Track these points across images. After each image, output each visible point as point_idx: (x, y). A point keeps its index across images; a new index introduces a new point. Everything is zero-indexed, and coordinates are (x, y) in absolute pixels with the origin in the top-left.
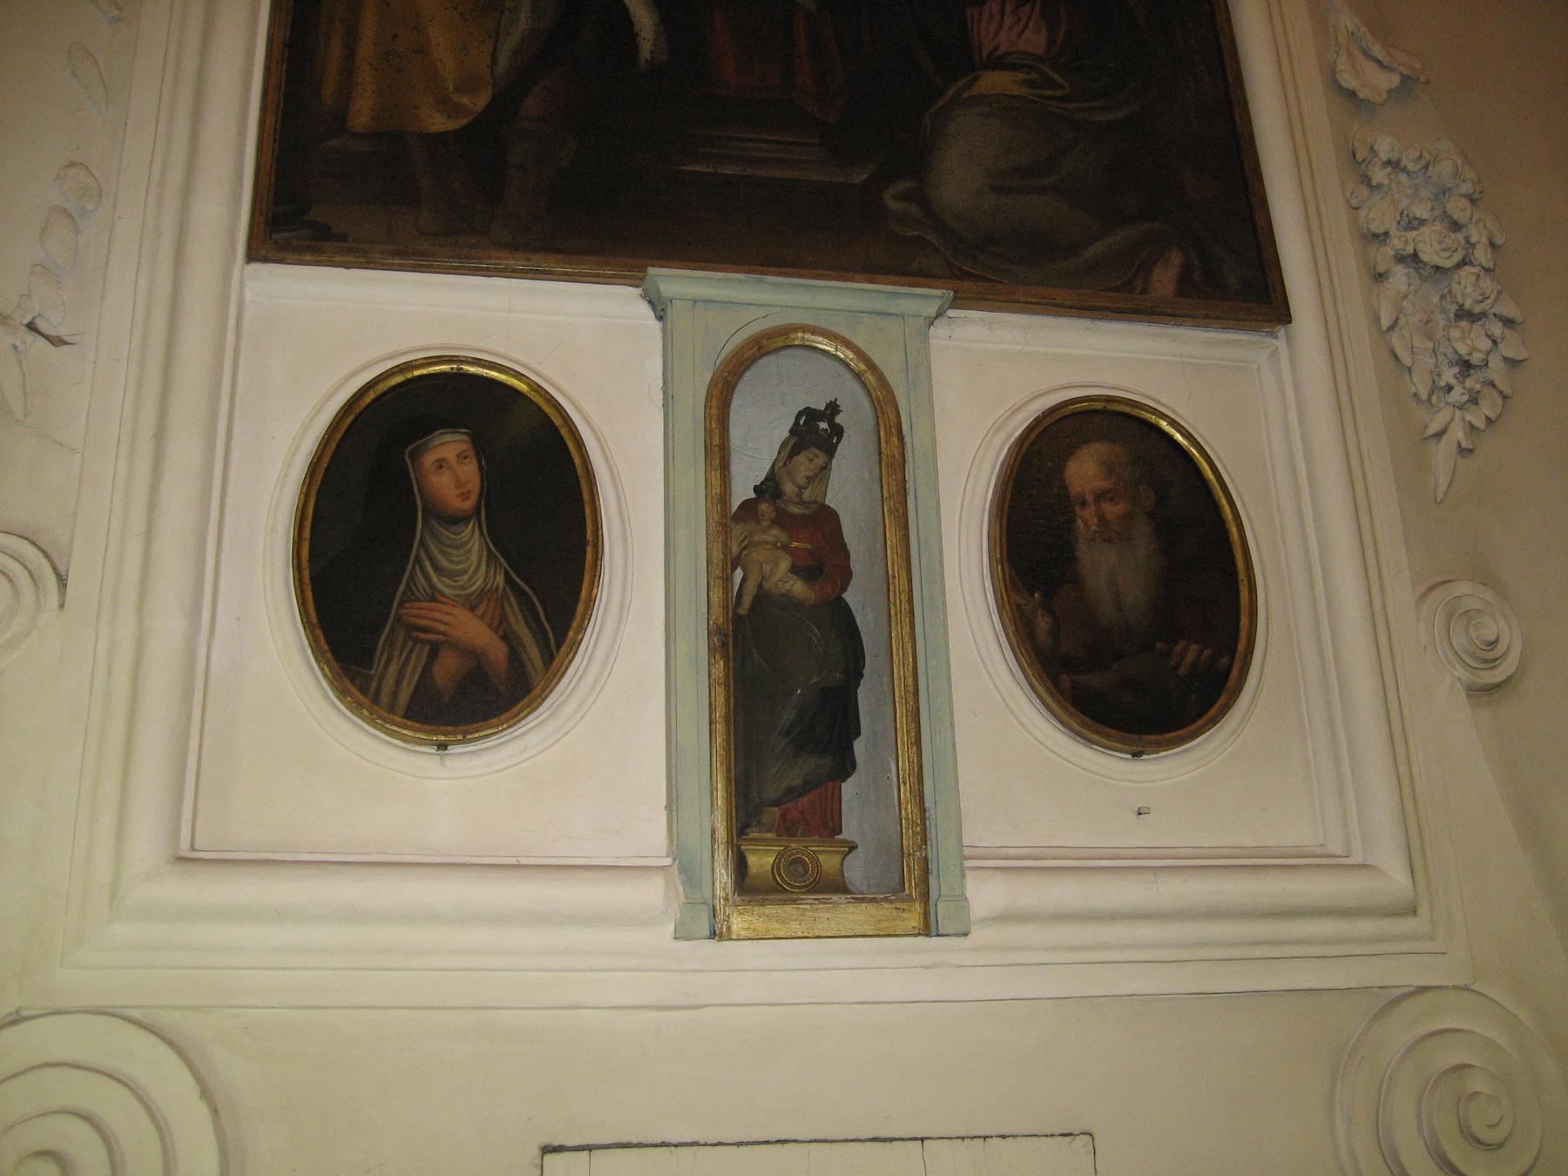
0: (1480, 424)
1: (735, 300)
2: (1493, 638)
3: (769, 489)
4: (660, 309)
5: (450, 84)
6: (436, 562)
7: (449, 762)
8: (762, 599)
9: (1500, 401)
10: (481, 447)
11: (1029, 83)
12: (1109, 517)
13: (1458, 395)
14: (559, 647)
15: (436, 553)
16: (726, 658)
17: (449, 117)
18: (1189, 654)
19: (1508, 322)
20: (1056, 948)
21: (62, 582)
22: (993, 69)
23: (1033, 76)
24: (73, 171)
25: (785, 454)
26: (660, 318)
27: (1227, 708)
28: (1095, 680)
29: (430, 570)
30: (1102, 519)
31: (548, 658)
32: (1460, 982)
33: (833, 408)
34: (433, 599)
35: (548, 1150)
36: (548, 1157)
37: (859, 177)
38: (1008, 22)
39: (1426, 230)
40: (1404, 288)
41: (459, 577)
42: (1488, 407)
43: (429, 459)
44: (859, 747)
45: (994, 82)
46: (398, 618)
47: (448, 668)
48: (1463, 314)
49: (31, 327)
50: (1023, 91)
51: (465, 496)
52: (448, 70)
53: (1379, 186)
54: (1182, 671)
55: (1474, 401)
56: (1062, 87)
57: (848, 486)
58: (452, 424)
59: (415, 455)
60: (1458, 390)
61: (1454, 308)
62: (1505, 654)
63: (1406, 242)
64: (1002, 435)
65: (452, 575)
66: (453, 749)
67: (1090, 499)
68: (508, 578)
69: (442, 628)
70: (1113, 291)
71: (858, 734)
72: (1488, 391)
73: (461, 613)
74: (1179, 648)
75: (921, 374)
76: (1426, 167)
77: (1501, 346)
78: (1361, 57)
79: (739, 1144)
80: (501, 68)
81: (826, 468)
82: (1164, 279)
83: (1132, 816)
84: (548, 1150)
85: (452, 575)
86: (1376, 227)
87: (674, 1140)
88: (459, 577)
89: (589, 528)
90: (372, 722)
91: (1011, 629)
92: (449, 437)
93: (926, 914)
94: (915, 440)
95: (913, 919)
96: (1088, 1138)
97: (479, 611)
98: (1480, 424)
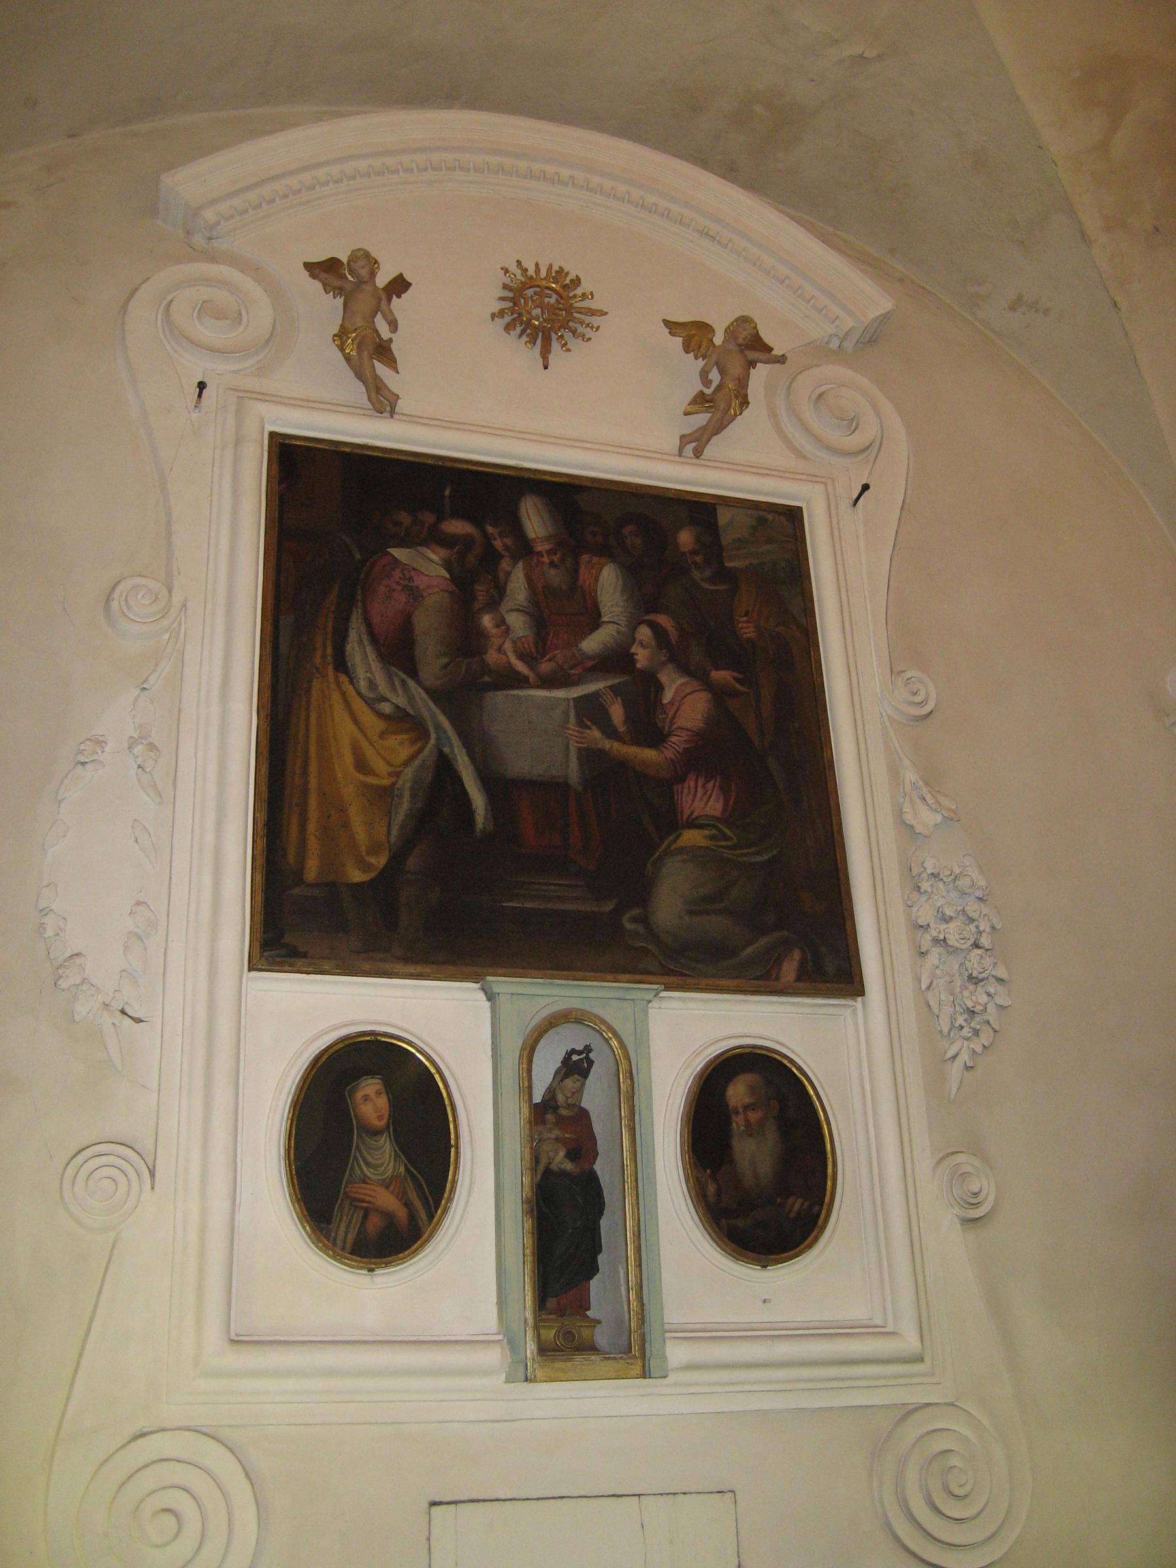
0: (979, 1049)
1: (536, 996)
2: (976, 1191)
3: (551, 1093)
4: (491, 997)
5: (363, 848)
6: (364, 1157)
7: (378, 1280)
8: (548, 1172)
9: (992, 1034)
10: (388, 1086)
11: (712, 838)
12: (752, 1121)
13: (966, 1032)
14: (437, 1209)
15: (366, 1154)
16: (532, 1217)
17: (364, 871)
18: (796, 1204)
19: (1000, 980)
20: (715, 1384)
21: (152, 1174)
22: (689, 828)
23: (714, 831)
24: (140, 908)
25: (558, 1078)
26: (489, 1000)
27: (816, 1239)
28: (740, 1223)
29: (362, 1163)
30: (747, 1121)
31: (431, 1217)
32: (950, 1400)
33: (588, 1049)
34: (364, 1182)
35: (434, 1504)
36: (435, 1509)
37: (609, 907)
38: (699, 794)
39: (952, 925)
40: (936, 962)
41: (379, 1164)
42: (985, 1038)
43: (360, 1095)
44: (601, 1259)
45: (691, 837)
46: (345, 1193)
47: (375, 1224)
48: (974, 980)
49: (123, 1012)
50: (708, 843)
51: (380, 1118)
52: (364, 844)
53: (926, 892)
54: (792, 1215)
55: (976, 1033)
56: (731, 839)
57: (595, 1096)
58: (371, 1073)
59: (352, 1093)
60: (966, 1030)
61: (967, 974)
62: (985, 1199)
63: (939, 932)
64: (689, 1071)
65: (375, 1167)
66: (378, 1272)
67: (741, 1110)
68: (407, 1170)
69: (368, 1198)
70: (759, 977)
71: (600, 1251)
72: (986, 1028)
73: (381, 1190)
74: (791, 1200)
75: (642, 1035)
76: (955, 880)
77: (996, 998)
78: (918, 801)
79: (538, 1499)
80: (393, 839)
81: (583, 1085)
82: (789, 970)
83: (761, 1303)
84: (434, 1504)
85: (375, 1167)
86: (921, 922)
87: (503, 1497)
88: (379, 1164)
89: (453, 1136)
90: (333, 1257)
91: (693, 1193)
92: (370, 1081)
93: (644, 1366)
94: (640, 1079)
95: (637, 1370)
96: (731, 1494)
97: (391, 1188)
98: (979, 1049)
